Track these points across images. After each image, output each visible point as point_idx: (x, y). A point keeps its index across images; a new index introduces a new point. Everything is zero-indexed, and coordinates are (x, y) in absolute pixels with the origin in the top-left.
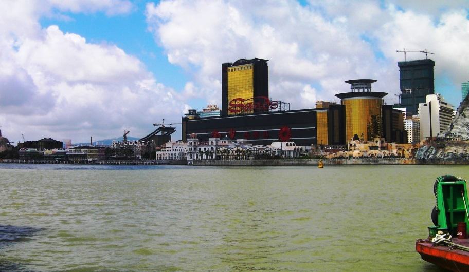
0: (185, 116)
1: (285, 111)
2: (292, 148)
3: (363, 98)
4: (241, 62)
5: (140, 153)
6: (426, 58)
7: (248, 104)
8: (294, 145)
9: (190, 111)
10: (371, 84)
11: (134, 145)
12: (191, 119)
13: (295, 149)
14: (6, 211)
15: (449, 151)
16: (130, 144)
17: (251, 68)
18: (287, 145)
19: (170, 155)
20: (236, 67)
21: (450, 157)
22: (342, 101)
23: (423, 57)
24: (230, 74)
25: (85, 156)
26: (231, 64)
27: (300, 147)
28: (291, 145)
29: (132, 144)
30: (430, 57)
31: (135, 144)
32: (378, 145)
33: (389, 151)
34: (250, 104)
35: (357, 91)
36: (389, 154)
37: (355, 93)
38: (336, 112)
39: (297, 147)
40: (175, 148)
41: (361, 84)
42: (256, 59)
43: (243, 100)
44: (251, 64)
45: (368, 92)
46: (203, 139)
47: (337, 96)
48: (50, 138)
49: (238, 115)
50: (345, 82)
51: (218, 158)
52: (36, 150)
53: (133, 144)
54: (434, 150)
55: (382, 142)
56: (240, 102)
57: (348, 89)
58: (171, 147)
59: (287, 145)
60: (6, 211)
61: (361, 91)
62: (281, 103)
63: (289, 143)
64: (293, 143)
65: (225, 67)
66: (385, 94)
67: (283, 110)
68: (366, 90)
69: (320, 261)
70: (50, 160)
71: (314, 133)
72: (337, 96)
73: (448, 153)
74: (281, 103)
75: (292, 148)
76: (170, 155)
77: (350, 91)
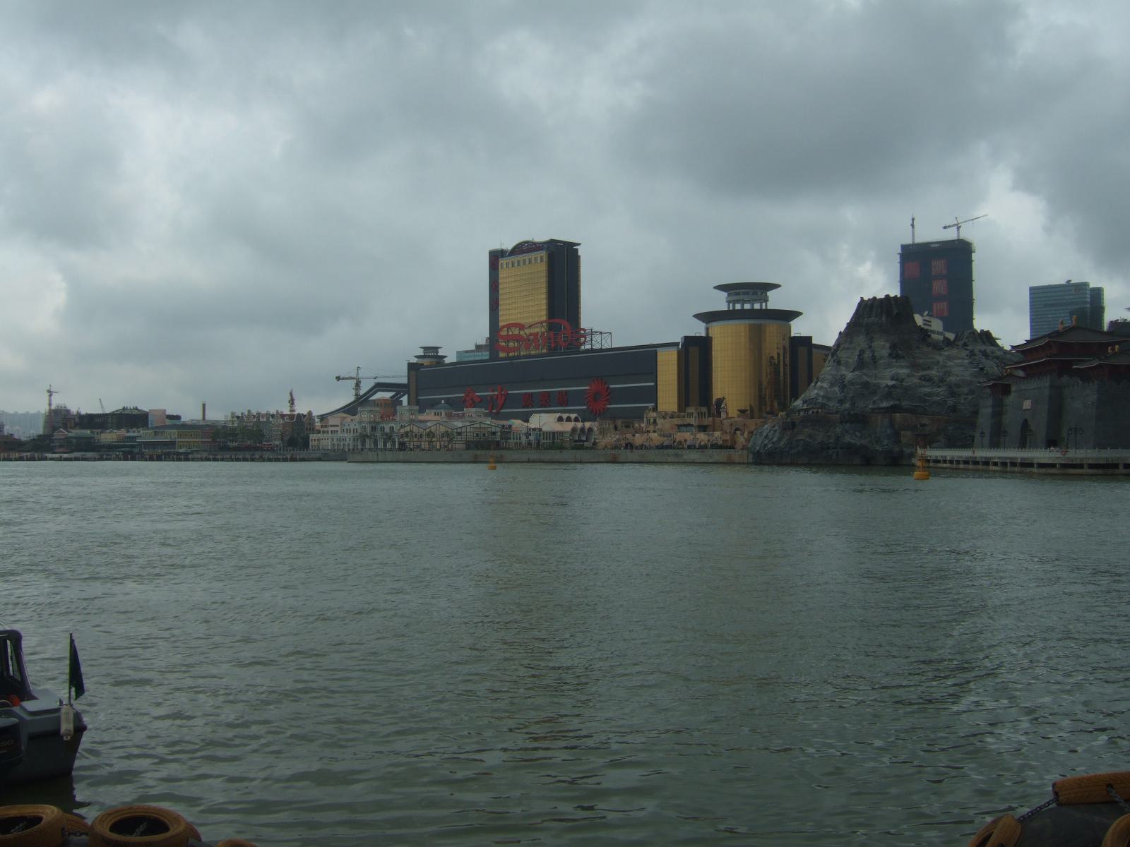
0: (415, 360)
1: (592, 350)
2: (568, 427)
3: (752, 322)
4: (524, 248)
5: (279, 437)
6: (956, 238)
7: (530, 334)
8: (576, 420)
9: (425, 348)
10: (769, 293)
11: (268, 422)
12: (427, 367)
13: (574, 430)
14: (828, 488)
15: (800, 437)
16: (261, 420)
17: (542, 261)
18: (560, 419)
19: (335, 440)
20: (515, 258)
21: (800, 448)
22: (707, 329)
23: (951, 235)
24: (502, 273)
25: (172, 444)
26: (506, 252)
27: (588, 425)
28: (569, 419)
29: (265, 420)
30: (966, 234)
31: (271, 419)
32: (692, 421)
33: (709, 435)
34: (536, 335)
35: (738, 307)
36: (709, 441)
37: (734, 311)
38: (694, 351)
39: (579, 425)
40: (346, 425)
41: (744, 293)
42: (552, 241)
43: (521, 327)
44: (544, 254)
45: (761, 310)
46: (421, 411)
47: (698, 316)
48: (136, 409)
49: (514, 358)
50: (715, 288)
51: (403, 445)
52: (89, 432)
53: (268, 419)
54: (777, 435)
55: (700, 414)
56: (516, 332)
57: (720, 302)
58: (339, 423)
59: (560, 419)
60: (828, 488)
61: (747, 306)
62: (592, 334)
63: (565, 416)
64: (573, 416)
65: (496, 258)
66: (795, 314)
67: (597, 346)
68: (757, 306)
69: (778, 634)
70: (130, 452)
71: (654, 391)
72: (698, 316)
73: (797, 440)
74: (592, 334)
75: (568, 427)
76: (335, 440)
77: (723, 306)
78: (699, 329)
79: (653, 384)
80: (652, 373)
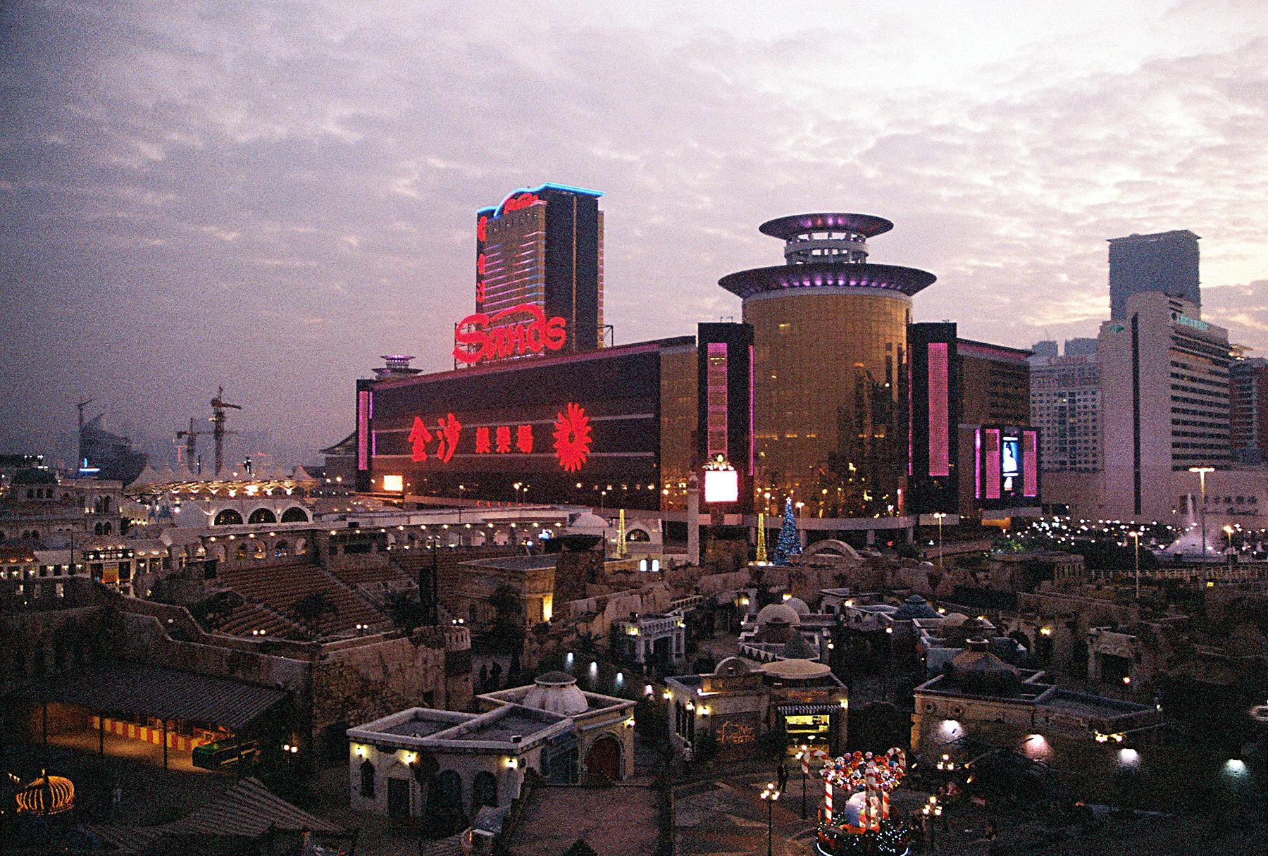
0: (374, 376)
57: (773, 253)
78: (730, 309)
79: (652, 416)
80: (653, 397)
